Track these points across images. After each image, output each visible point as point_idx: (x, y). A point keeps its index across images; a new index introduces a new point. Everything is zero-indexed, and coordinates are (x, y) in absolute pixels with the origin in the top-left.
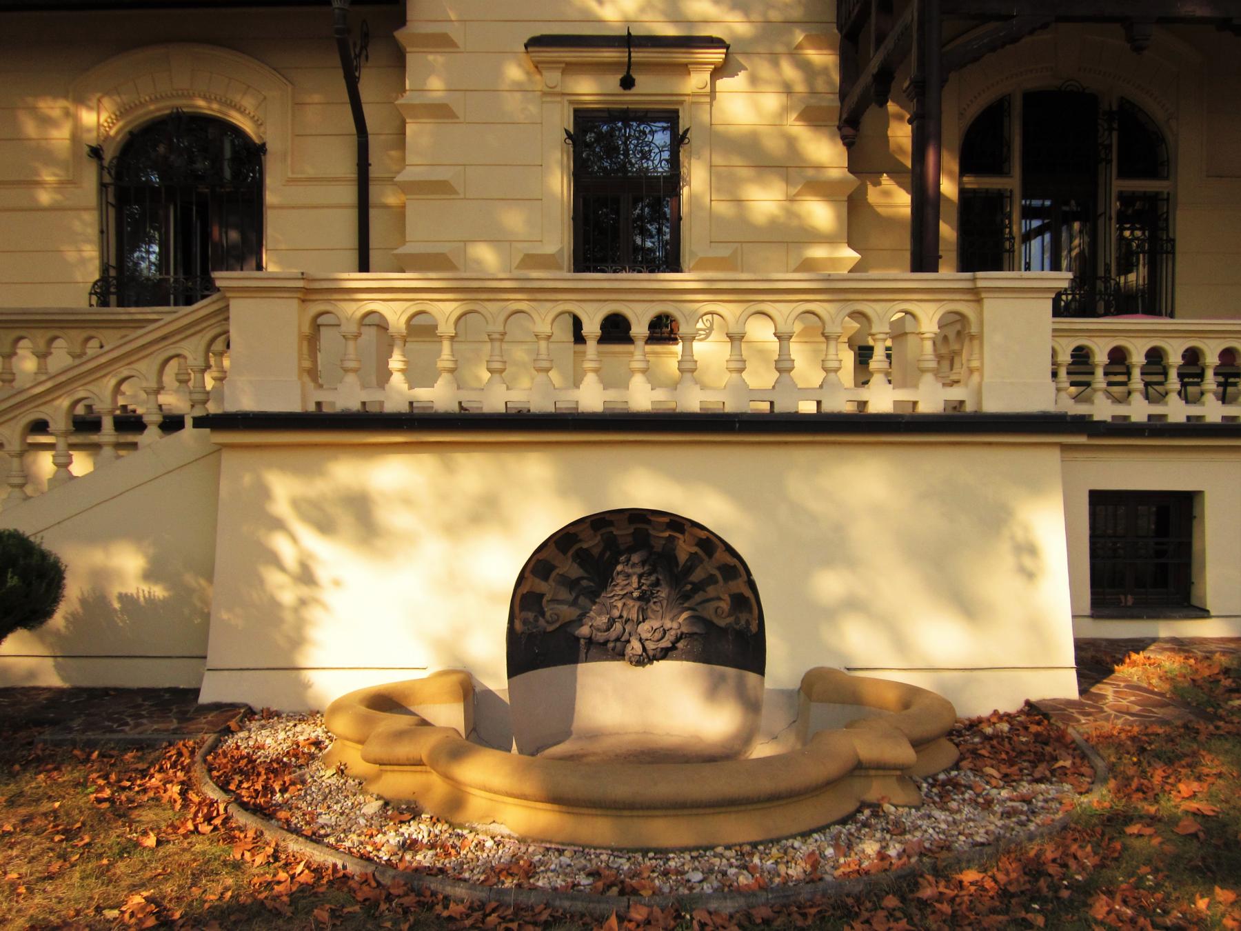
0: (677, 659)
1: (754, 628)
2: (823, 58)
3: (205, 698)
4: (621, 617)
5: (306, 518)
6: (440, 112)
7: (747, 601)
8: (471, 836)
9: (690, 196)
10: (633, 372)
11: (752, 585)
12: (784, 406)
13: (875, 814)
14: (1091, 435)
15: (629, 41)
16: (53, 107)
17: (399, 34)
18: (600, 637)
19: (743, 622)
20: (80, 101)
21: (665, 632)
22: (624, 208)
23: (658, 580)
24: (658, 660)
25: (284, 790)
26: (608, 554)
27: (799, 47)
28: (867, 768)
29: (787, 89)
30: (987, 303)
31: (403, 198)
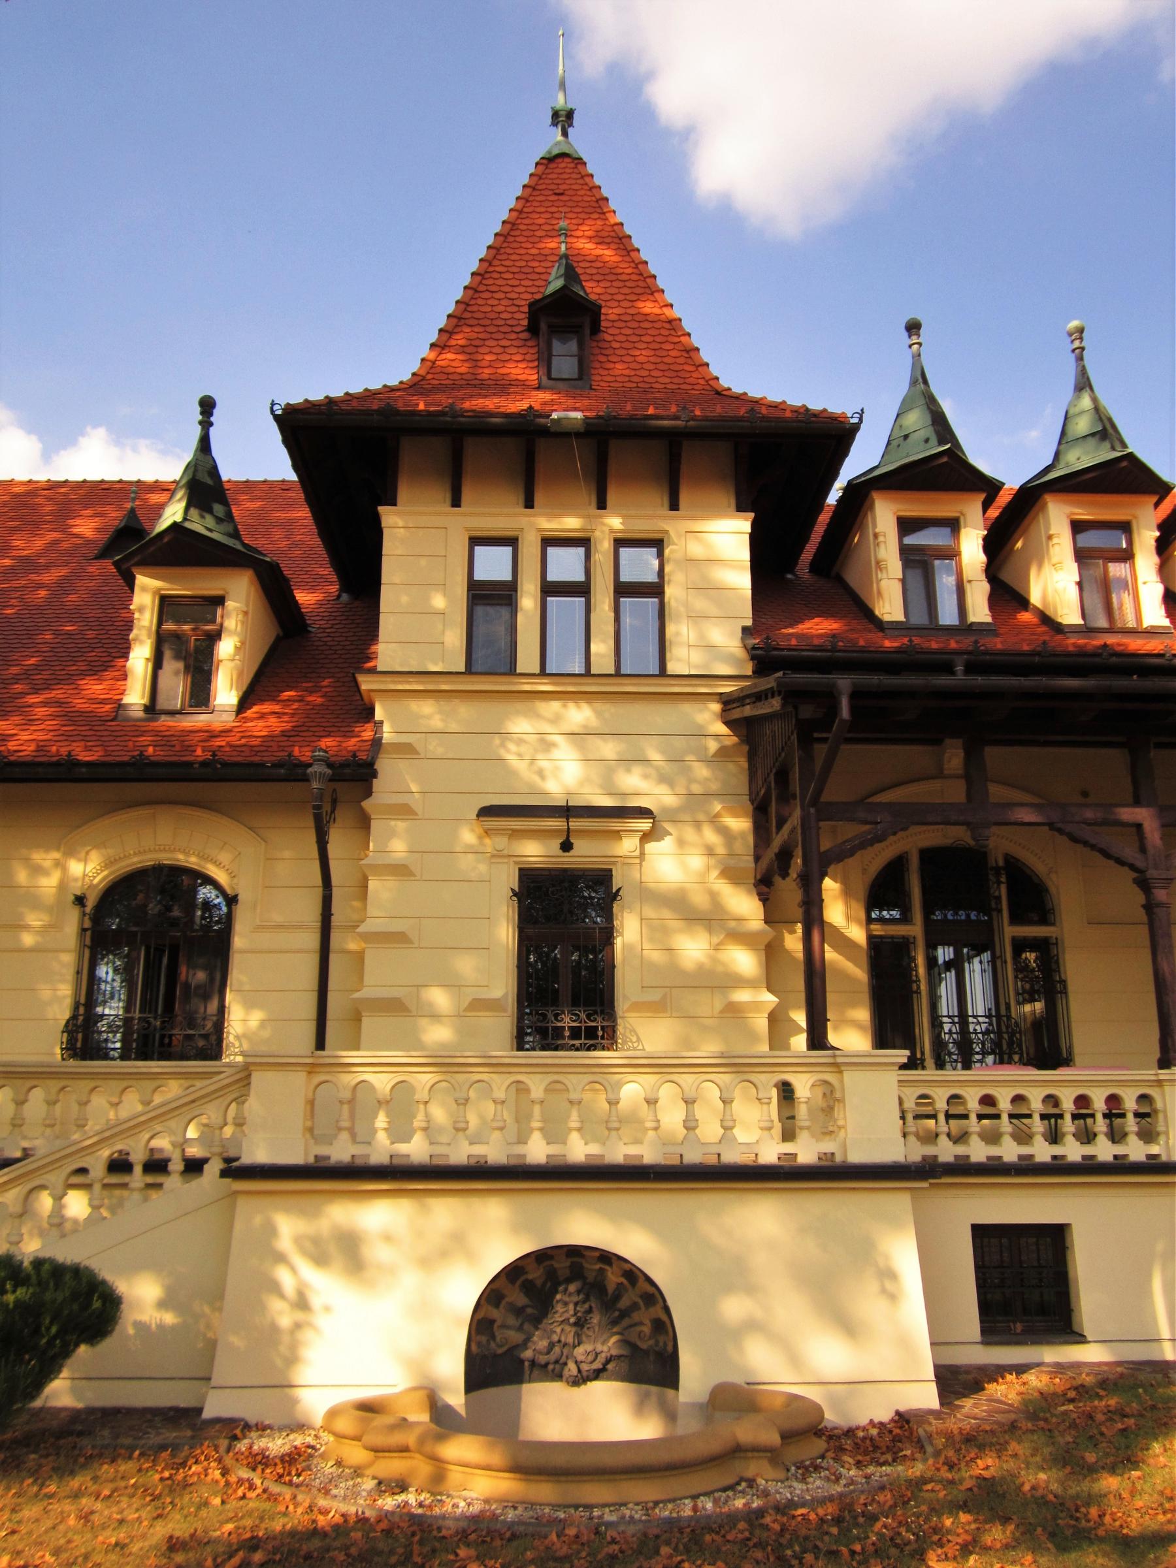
0: (608, 1379)
1: (670, 1348)
2: (740, 824)
3: (207, 1414)
4: (559, 1341)
5: (305, 1253)
6: (401, 871)
7: (664, 1326)
8: (448, 1500)
9: (624, 945)
10: (570, 1130)
11: (667, 1309)
13: (751, 1486)
15: (567, 811)
16: (45, 858)
17: (365, 804)
18: (542, 1359)
19: (661, 1344)
20: (70, 853)
21: (597, 1355)
22: (565, 969)
23: (591, 1307)
24: (591, 1380)
25: (299, 1475)
26: (549, 1284)
27: (718, 815)
28: (747, 1450)
29: (710, 852)
30: (846, 1075)
31: (364, 945)
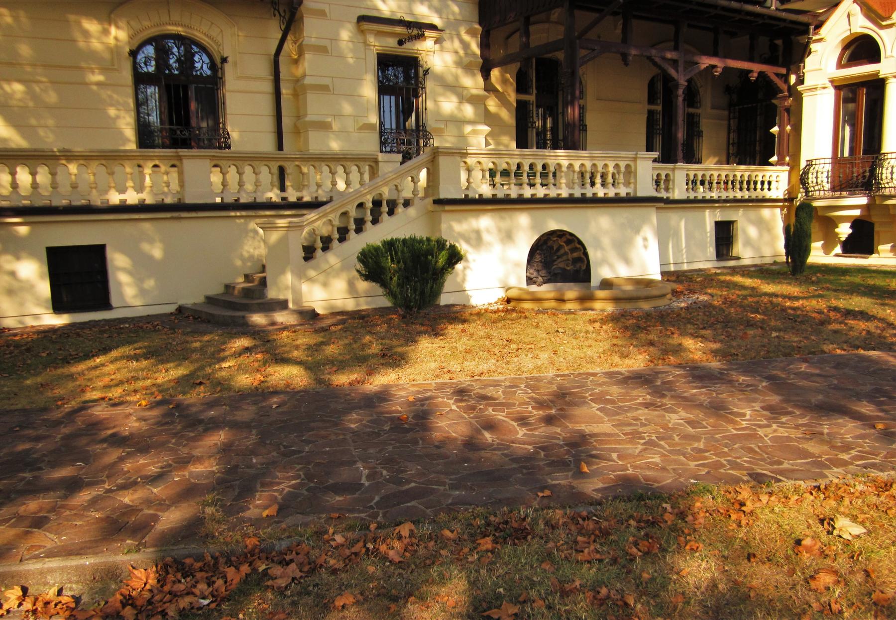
12: (55, 203)
14: (665, 203)
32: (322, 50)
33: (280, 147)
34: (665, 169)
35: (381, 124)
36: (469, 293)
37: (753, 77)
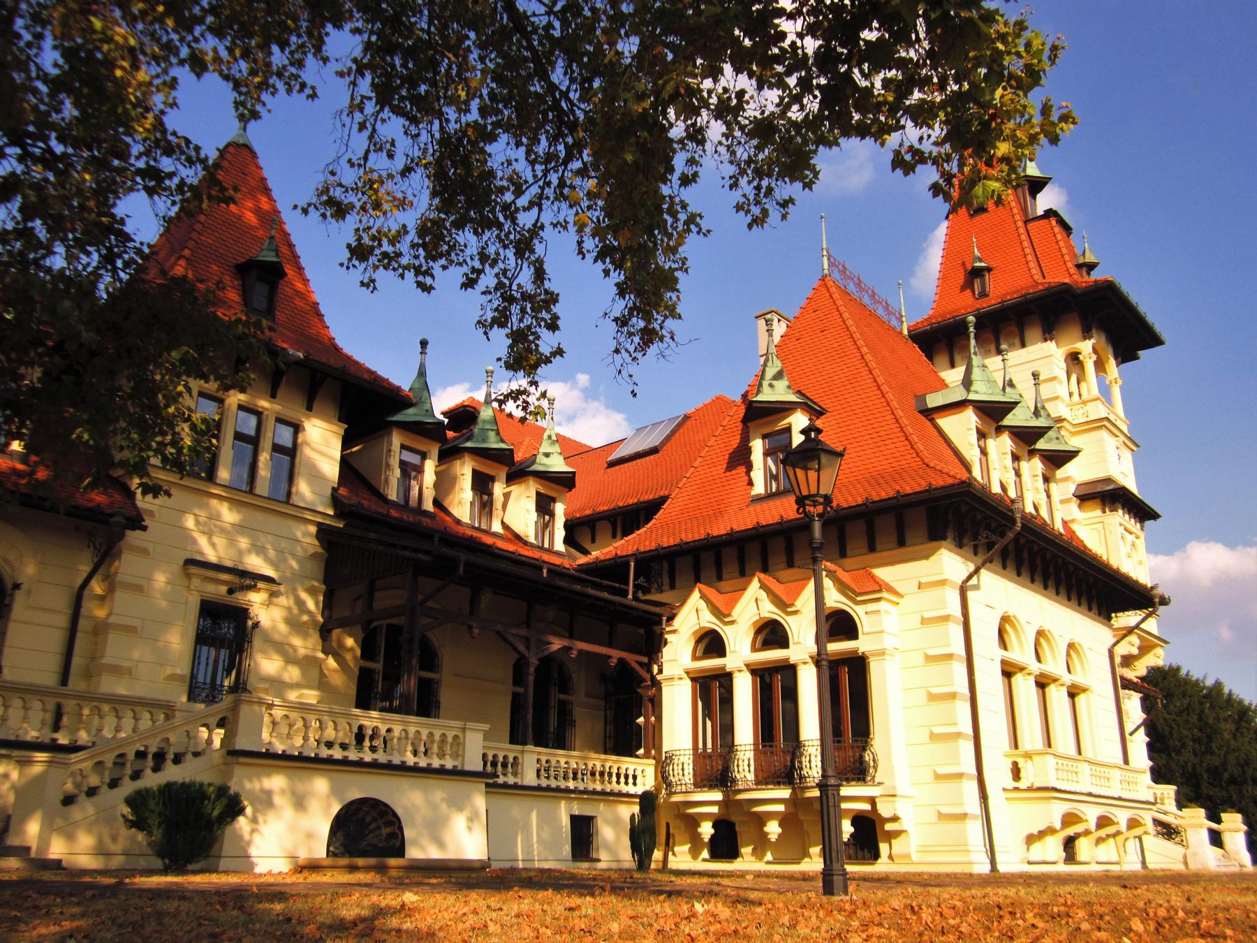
32: (138, 589)
33: (64, 680)
34: (514, 751)
35: (193, 676)
36: (254, 860)
37: (613, 663)
